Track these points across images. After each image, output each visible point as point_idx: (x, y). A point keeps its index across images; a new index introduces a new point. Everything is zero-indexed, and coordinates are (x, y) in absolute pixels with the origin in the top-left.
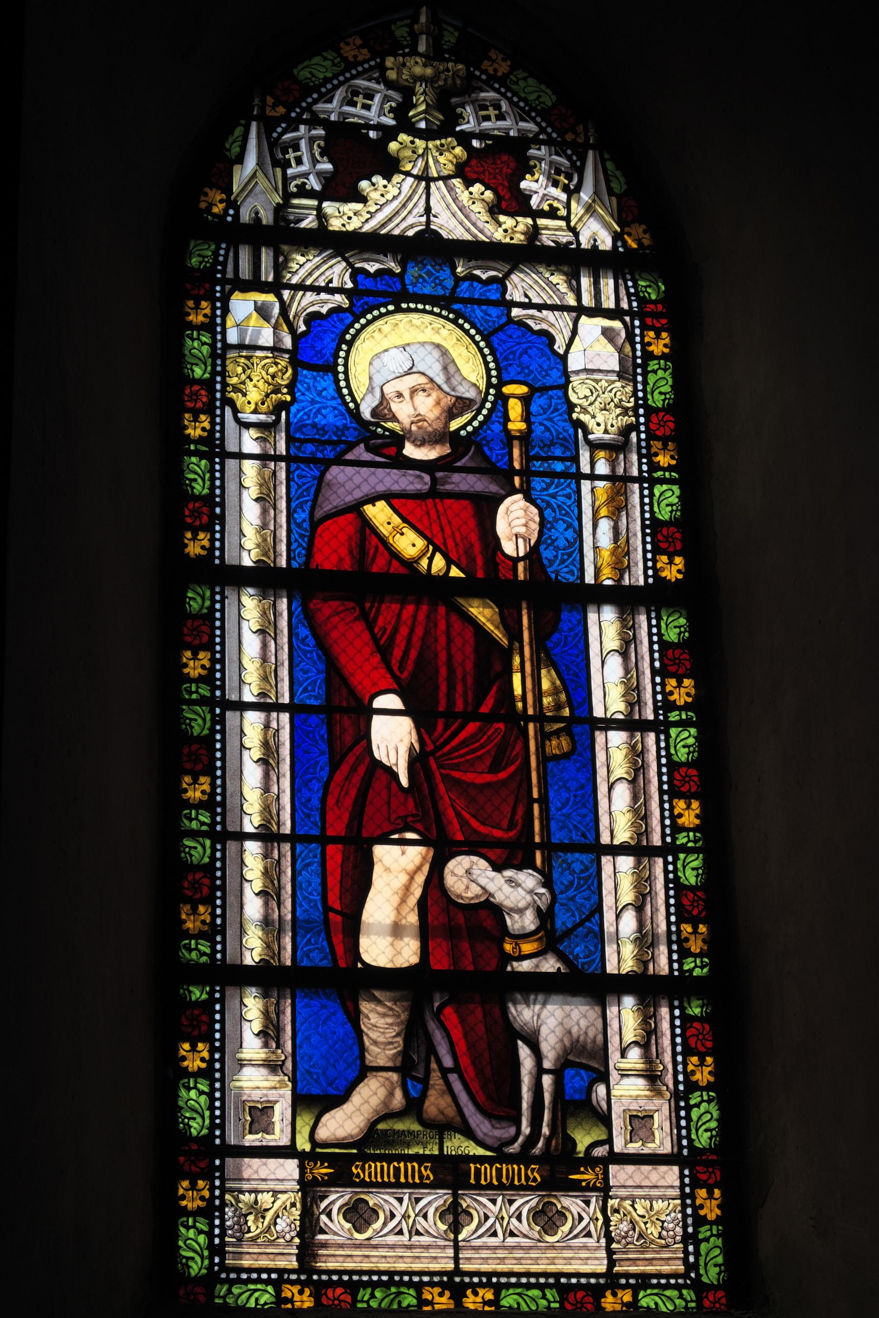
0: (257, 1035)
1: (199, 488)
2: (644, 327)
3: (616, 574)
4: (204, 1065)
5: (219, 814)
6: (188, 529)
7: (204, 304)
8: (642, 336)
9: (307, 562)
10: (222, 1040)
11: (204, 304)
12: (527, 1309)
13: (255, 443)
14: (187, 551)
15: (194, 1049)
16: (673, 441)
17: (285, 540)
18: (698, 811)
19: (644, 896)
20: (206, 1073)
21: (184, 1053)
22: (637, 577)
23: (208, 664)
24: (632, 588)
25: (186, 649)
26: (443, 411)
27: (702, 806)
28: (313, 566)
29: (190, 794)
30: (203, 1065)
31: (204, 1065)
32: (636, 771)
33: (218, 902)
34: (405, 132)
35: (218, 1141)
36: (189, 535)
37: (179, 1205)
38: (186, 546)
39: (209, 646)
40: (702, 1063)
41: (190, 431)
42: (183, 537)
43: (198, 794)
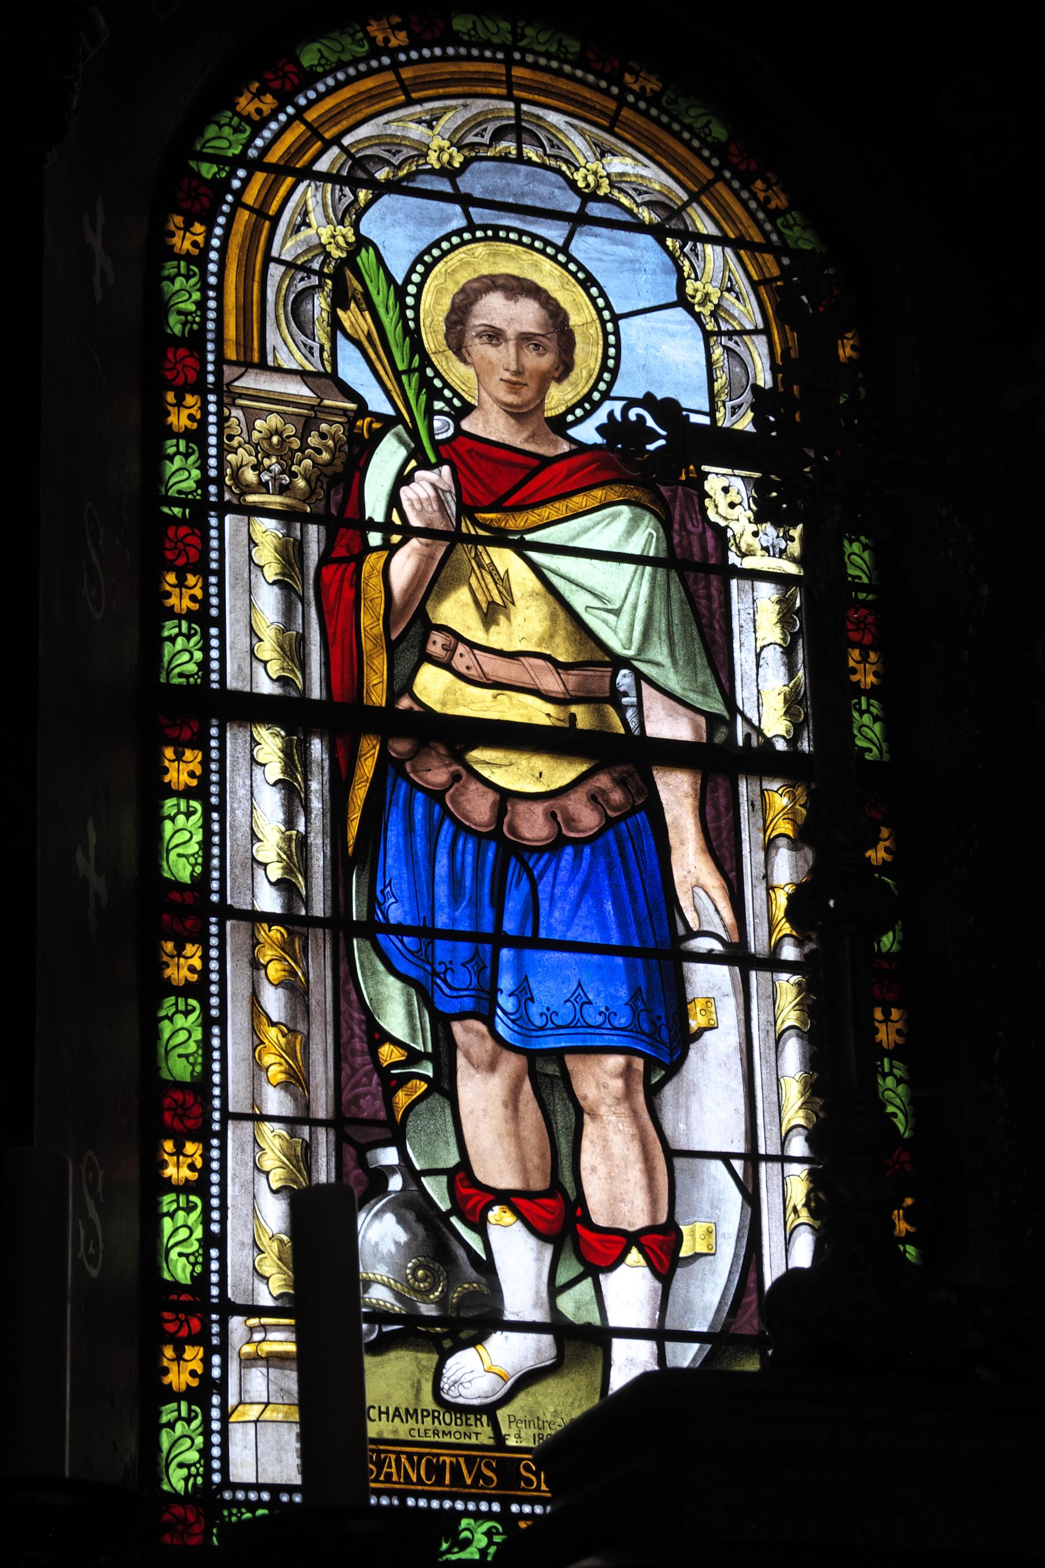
0: (275, 784)
1: (180, 1069)
4: (195, 607)
5: (223, 214)
6: (170, 569)
9: (296, 1423)
10: (222, 795)
15: (181, 584)
17: (322, 111)
18: (898, 1026)
21: (168, 588)
25: (168, 1137)
26: (478, 1072)
27: (908, 1021)
28: (313, 1183)
29: (173, 601)
31: (194, 978)
33: (214, 941)
35: (215, 898)
36: (169, 1146)
37: (163, 605)
39: (202, 569)
42: (161, 756)
43: (187, 245)
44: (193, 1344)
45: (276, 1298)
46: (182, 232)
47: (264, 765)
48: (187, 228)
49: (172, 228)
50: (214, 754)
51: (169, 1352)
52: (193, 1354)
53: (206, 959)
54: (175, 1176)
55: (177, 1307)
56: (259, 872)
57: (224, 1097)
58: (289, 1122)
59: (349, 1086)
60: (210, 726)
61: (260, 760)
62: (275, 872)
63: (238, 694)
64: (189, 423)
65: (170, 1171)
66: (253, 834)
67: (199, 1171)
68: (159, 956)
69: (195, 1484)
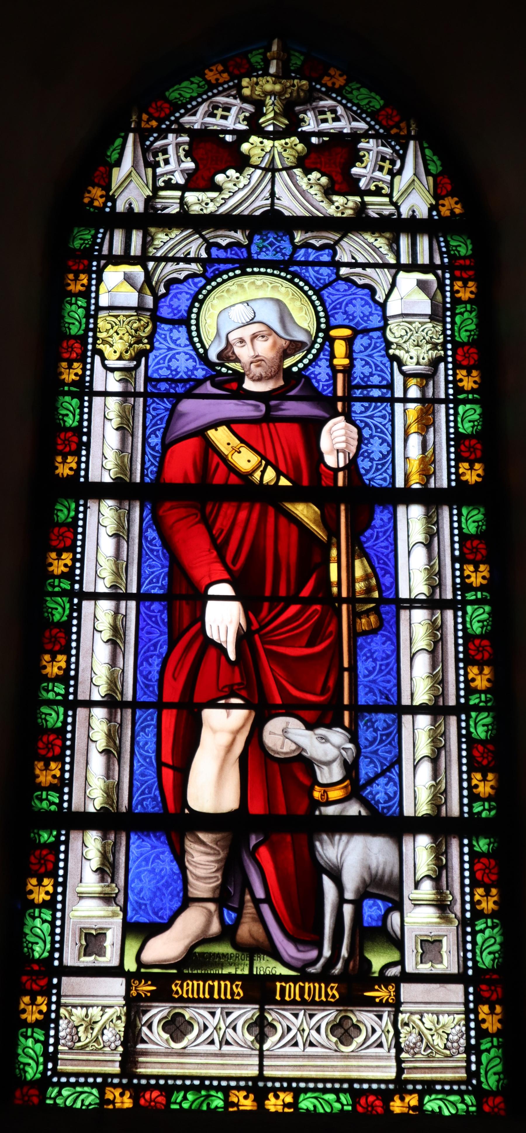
0: (96, 871)
4: (48, 898)
19: (439, 749)
20: (50, 905)
25: (58, 455)
36: (59, 459)
39: (72, 549)
41: (65, 376)
42: (54, 460)
43: (55, 670)
44: (72, 455)
45: (102, 697)
46: (44, 772)
47: (96, 741)
48: (53, 659)
49: (44, 663)
50: (84, 459)
51: (59, 459)
52: (67, 558)
53: (84, 369)
54: (67, 379)
55: (32, 973)
56: (86, 864)
57: (97, 298)
58: (124, 395)
59: (147, 582)
60: (82, 450)
61: (94, 739)
62: (111, 530)
63: (78, 813)
64: (74, 377)
65: (72, 288)
66: (95, 617)
67: (70, 567)
68: (54, 464)
69: (85, 247)
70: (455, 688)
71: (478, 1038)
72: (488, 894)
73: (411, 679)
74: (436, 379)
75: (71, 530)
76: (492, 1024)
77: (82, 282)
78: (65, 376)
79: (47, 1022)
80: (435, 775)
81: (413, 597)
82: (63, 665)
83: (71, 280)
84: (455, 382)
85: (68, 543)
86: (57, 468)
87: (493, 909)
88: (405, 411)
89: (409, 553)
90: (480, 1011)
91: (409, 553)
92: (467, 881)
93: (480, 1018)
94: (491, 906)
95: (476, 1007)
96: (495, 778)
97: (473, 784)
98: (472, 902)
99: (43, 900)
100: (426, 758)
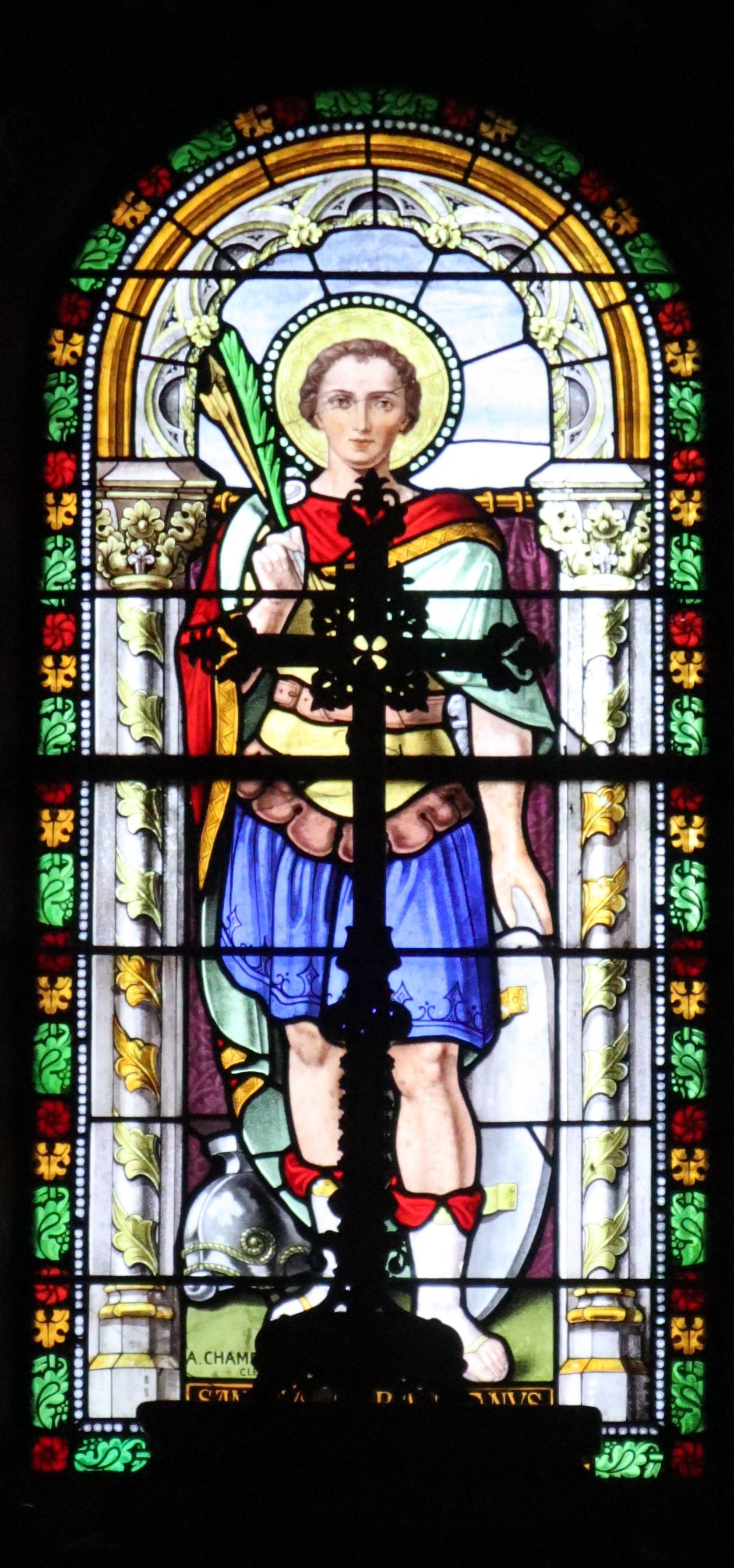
2: (671, 485)
3: (610, 1001)
7: (66, 660)
8: (666, 500)
11: (66, 660)
12: (451, 752)
13: (140, 744)
14: (38, 1338)
16: (700, 814)
19: (619, 1083)
20: (72, 846)
22: (639, 744)
23: (78, 350)
24: (633, 758)
30: (64, 1006)
32: (619, 1083)
34: (350, 983)
36: (42, 1148)
38: (53, 348)
39: (75, 650)
40: (684, 350)
41: (50, 682)
70: (646, 370)
71: (666, 383)
72: (689, 1326)
73: (582, 1055)
74: (631, 832)
75: (71, 617)
76: (686, 366)
77: (67, 671)
78: (50, 682)
79: (70, 1345)
80: (615, 1031)
81: (585, 1277)
82: (68, 994)
83: (51, 668)
84: (667, 674)
85: (69, 476)
86: (46, 677)
87: (696, 1181)
88: (582, 794)
89: (583, 1196)
90: (672, 990)
91: (583, 1196)
92: (661, 807)
93: (673, 999)
94: (695, 1343)
95: (667, 984)
96: (706, 1154)
97: (673, 1001)
98: (667, 511)
99: (64, 525)
100: (601, 1097)
